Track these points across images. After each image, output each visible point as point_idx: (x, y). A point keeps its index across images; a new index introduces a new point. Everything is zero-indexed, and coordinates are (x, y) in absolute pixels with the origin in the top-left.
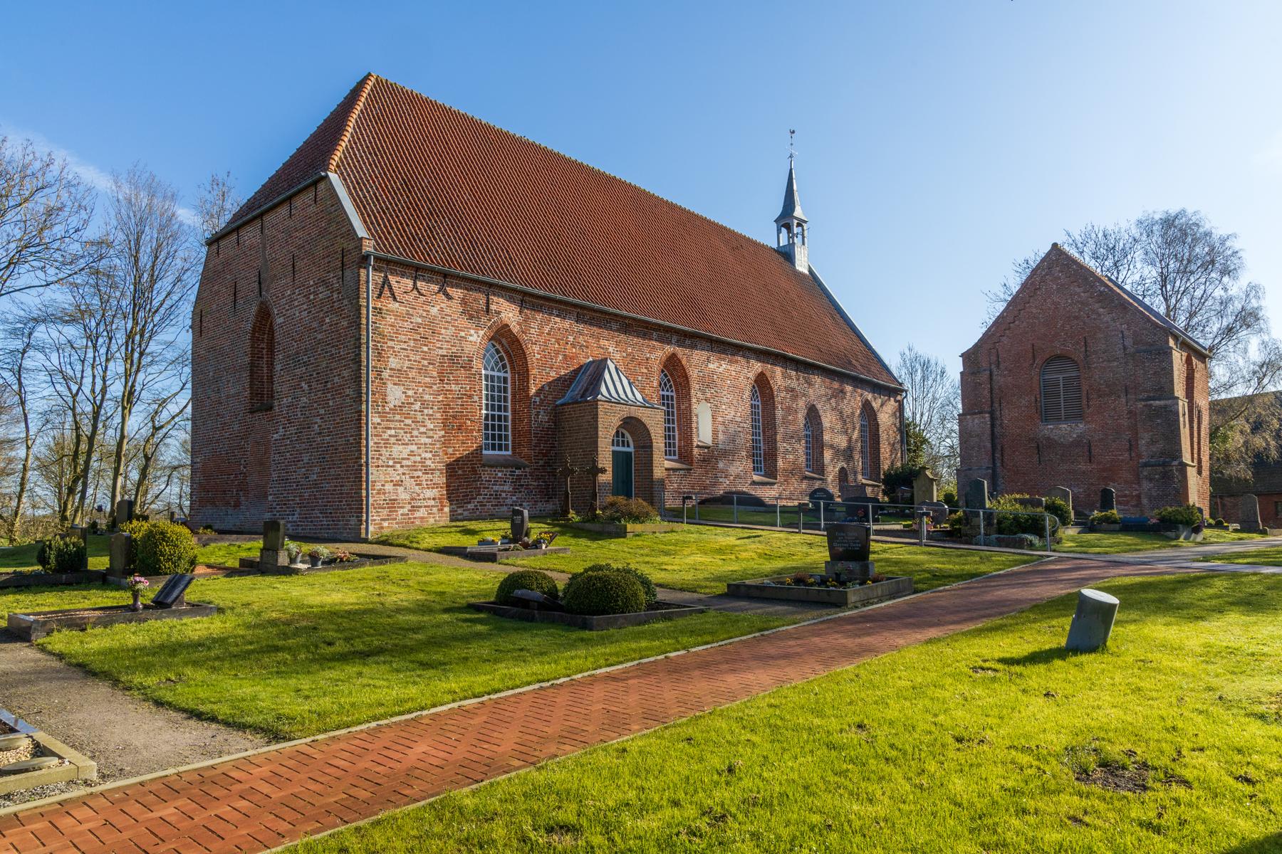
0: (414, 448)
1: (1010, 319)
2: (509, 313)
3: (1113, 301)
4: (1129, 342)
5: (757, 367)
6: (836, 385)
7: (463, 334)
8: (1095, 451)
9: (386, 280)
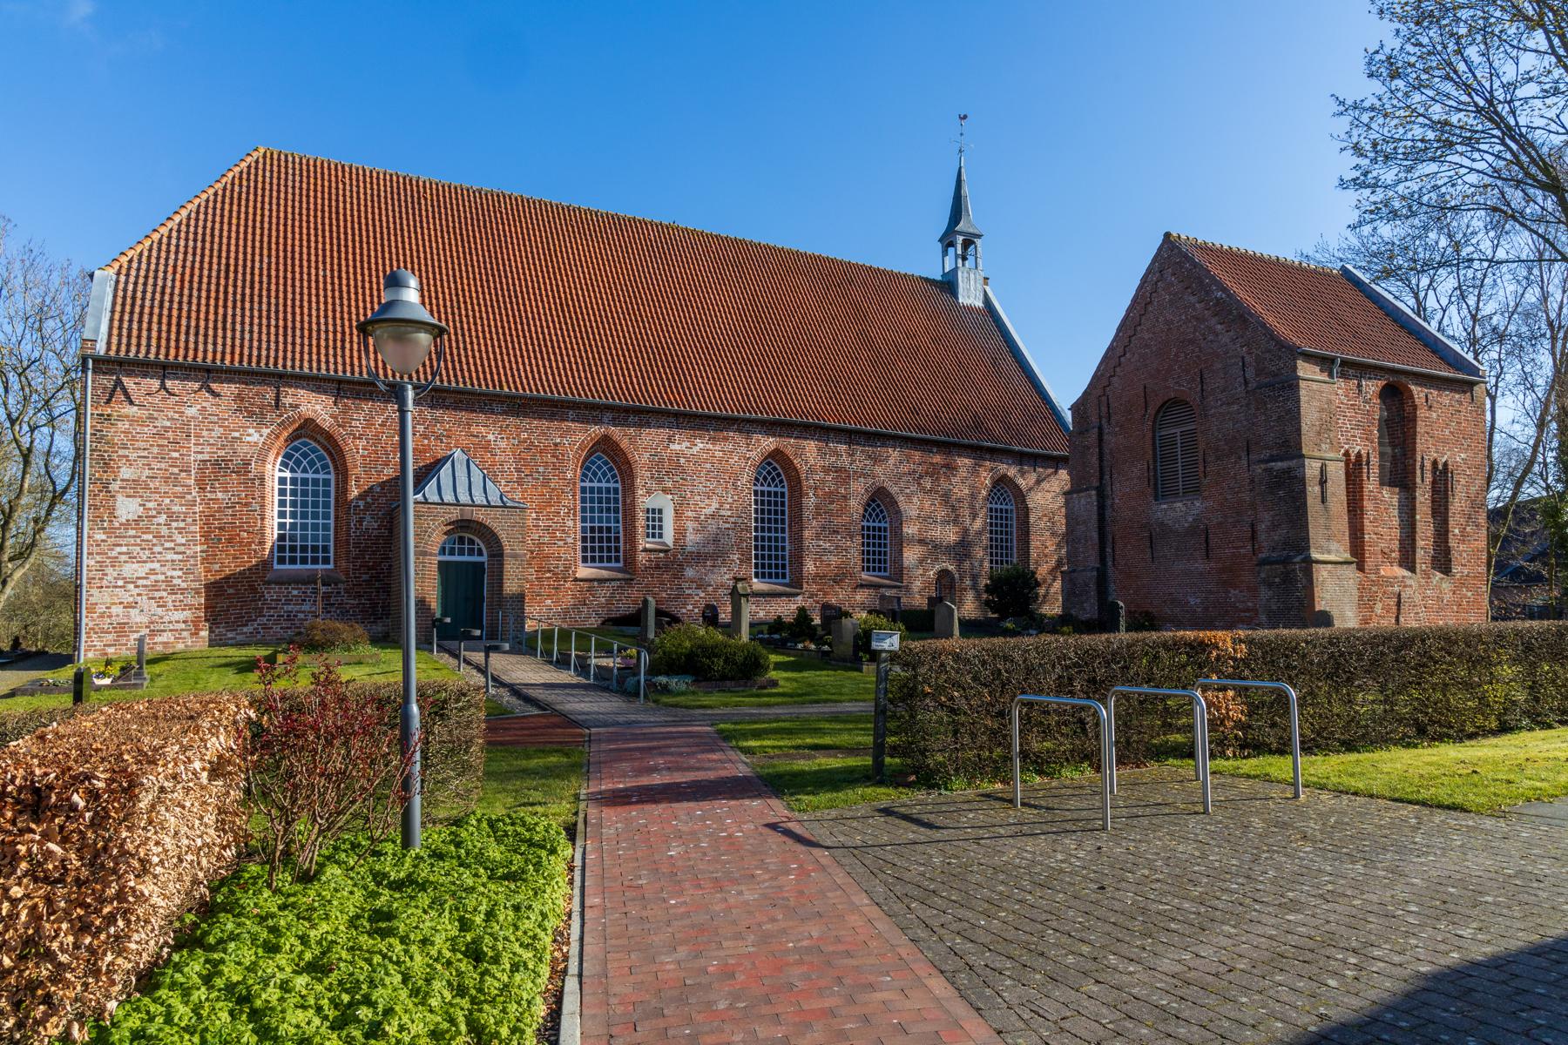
0: (156, 566)
1: (1120, 351)
2: (317, 407)
3: (1230, 312)
4: (1250, 373)
5: (769, 443)
6: (937, 459)
7: (236, 434)
8: (1214, 541)
9: (119, 383)
